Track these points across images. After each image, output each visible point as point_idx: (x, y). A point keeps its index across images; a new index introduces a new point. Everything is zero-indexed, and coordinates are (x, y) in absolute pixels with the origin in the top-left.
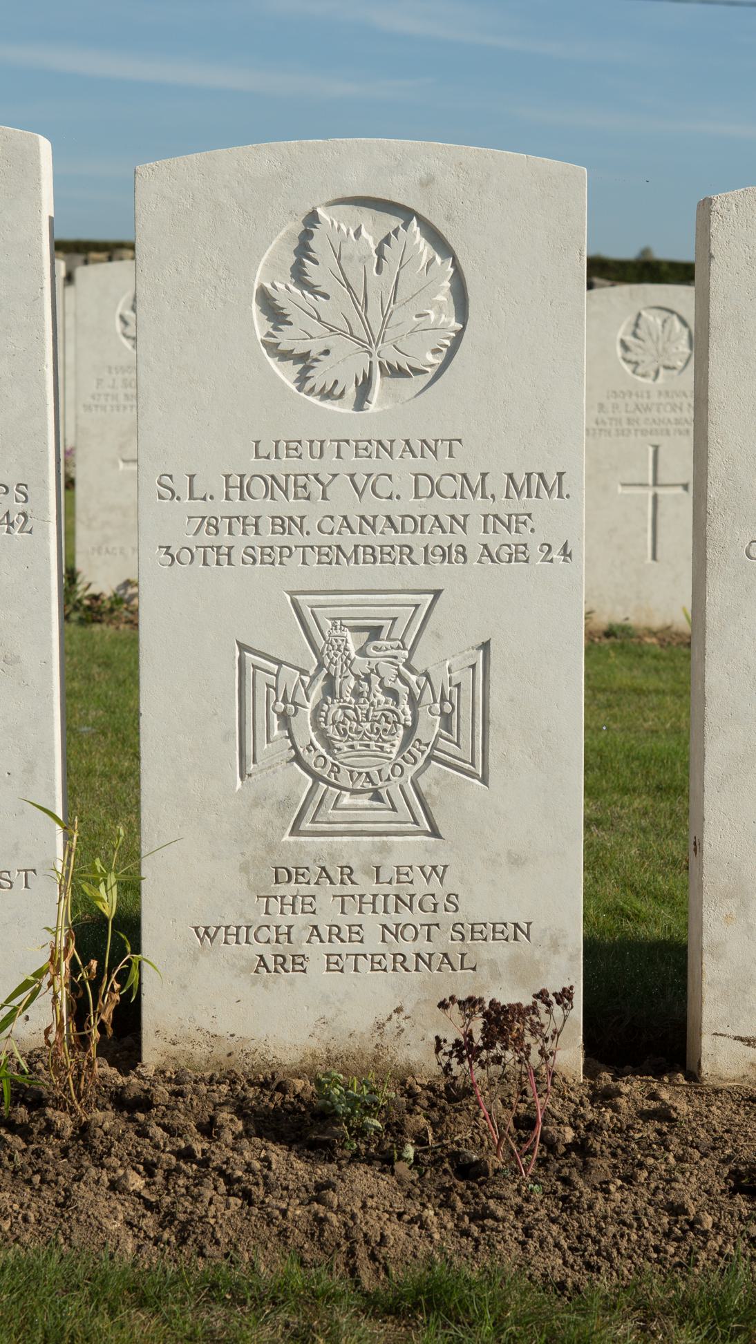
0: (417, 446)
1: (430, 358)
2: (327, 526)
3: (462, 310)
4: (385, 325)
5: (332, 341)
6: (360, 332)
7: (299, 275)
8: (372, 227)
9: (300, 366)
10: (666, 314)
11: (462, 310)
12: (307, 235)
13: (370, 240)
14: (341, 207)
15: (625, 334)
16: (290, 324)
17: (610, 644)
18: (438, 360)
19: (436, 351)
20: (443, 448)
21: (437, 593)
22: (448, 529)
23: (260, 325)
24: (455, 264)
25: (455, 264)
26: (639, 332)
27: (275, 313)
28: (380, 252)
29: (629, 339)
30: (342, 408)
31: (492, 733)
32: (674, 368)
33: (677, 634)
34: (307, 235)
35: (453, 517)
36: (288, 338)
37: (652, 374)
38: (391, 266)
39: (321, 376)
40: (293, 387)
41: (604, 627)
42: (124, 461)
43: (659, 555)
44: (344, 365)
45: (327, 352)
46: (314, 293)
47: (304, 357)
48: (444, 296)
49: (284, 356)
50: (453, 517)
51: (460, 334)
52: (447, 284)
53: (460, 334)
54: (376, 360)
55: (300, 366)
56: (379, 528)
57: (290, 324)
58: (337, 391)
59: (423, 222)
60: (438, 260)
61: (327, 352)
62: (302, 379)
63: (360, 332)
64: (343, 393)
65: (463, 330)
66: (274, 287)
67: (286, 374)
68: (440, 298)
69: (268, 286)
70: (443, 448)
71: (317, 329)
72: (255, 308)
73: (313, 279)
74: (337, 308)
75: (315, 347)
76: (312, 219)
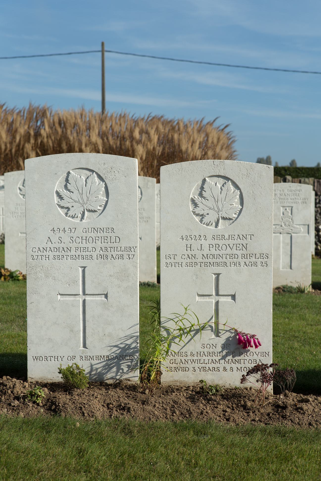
0: (241, 236)
2: (34, 250)
3: (242, 203)
4: (223, 207)
5: (74, 204)
6: (216, 209)
9: (201, 217)
11: (242, 203)
12: (68, 177)
13: (219, 186)
14: (77, 170)
16: (199, 207)
17: (143, 285)
18: (236, 216)
20: (248, 237)
22: (66, 251)
23: (191, 207)
24: (241, 192)
25: (241, 192)
28: (86, 181)
29: (21, 187)
30: (213, 227)
32: (95, 211)
33: (289, 287)
34: (68, 177)
35: (43, 248)
36: (198, 211)
37: (214, 224)
38: (224, 192)
39: (205, 220)
40: (64, 215)
42: (21, 233)
44: (212, 217)
45: (208, 214)
46: (70, 192)
49: (197, 215)
50: (43, 248)
51: (241, 210)
52: (238, 197)
54: (220, 216)
55: (201, 217)
56: (48, 251)
57: (199, 207)
58: (76, 216)
59: (97, 173)
60: (101, 183)
61: (208, 214)
62: (201, 221)
63: (81, 201)
64: (212, 224)
65: (108, 200)
66: (195, 197)
68: (236, 200)
69: (58, 190)
70: (248, 237)
72: (55, 195)
73: (69, 188)
74: (211, 203)
75: (205, 213)
76: (69, 173)
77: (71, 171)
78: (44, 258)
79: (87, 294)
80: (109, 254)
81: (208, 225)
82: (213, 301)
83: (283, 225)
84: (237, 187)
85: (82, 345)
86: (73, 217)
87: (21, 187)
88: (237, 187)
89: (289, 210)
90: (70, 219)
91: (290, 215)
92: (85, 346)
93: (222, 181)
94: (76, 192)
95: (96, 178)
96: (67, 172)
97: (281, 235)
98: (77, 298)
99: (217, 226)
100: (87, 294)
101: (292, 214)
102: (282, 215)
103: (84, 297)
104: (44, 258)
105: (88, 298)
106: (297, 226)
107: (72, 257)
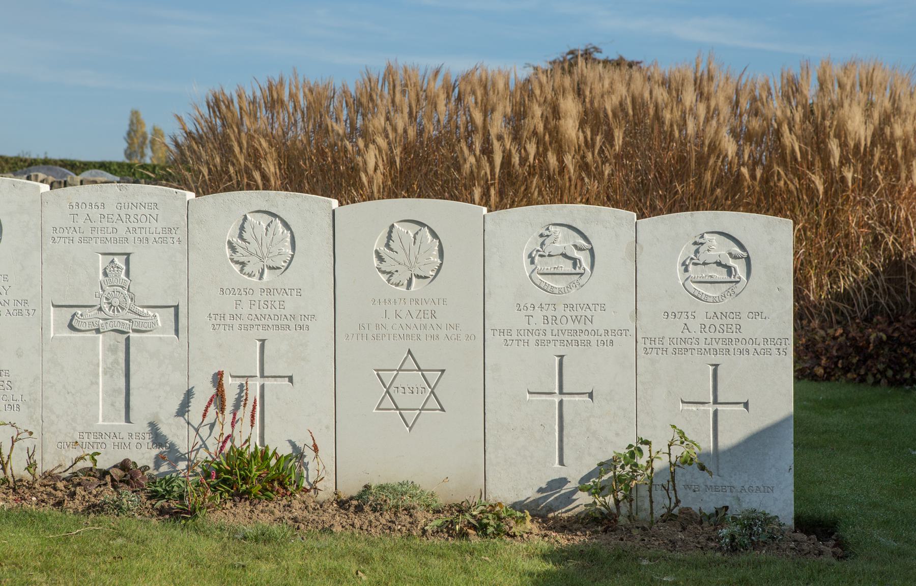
1: (431, 273)
7: (241, 237)
8: (411, 229)
10: (418, 227)
12: (390, 232)
15: (232, 237)
18: (285, 265)
19: (285, 262)
21: (443, 371)
24: (292, 233)
26: (245, 235)
27: (381, 259)
29: (236, 240)
30: (403, 289)
31: (719, 434)
32: (426, 277)
34: (390, 232)
36: (384, 267)
37: (258, 275)
39: (247, 269)
41: (350, 488)
43: (565, 461)
47: (390, 273)
48: (436, 252)
49: (384, 272)
51: (441, 264)
53: (441, 264)
67: (236, 268)
71: (393, 262)
74: (401, 257)
75: (393, 269)
76: (393, 226)
77: (248, 216)
78: (521, 343)
79: (268, 377)
80: (731, 348)
81: (397, 285)
82: (556, 399)
83: (106, 307)
84: (434, 235)
85: (557, 461)
86: (250, 275)
87: (236, 240)
88: (286, 225)
89: (119, 261)
90: (246, 277)
91: (123, 276)
92: (561, 462)
93: (269, 218)
94: (401, 251)
95: (280, 225)
96: (390, 224)
97: (101, 336)
98: (705, 407)
99: (261, 278)
100: (268, 377)
101: (128, 274)
102: (101, 277)
103: (262, 381)
104: (521, 343)
105: (566, 398)
106: (145, 310)
107: (700, 351)
